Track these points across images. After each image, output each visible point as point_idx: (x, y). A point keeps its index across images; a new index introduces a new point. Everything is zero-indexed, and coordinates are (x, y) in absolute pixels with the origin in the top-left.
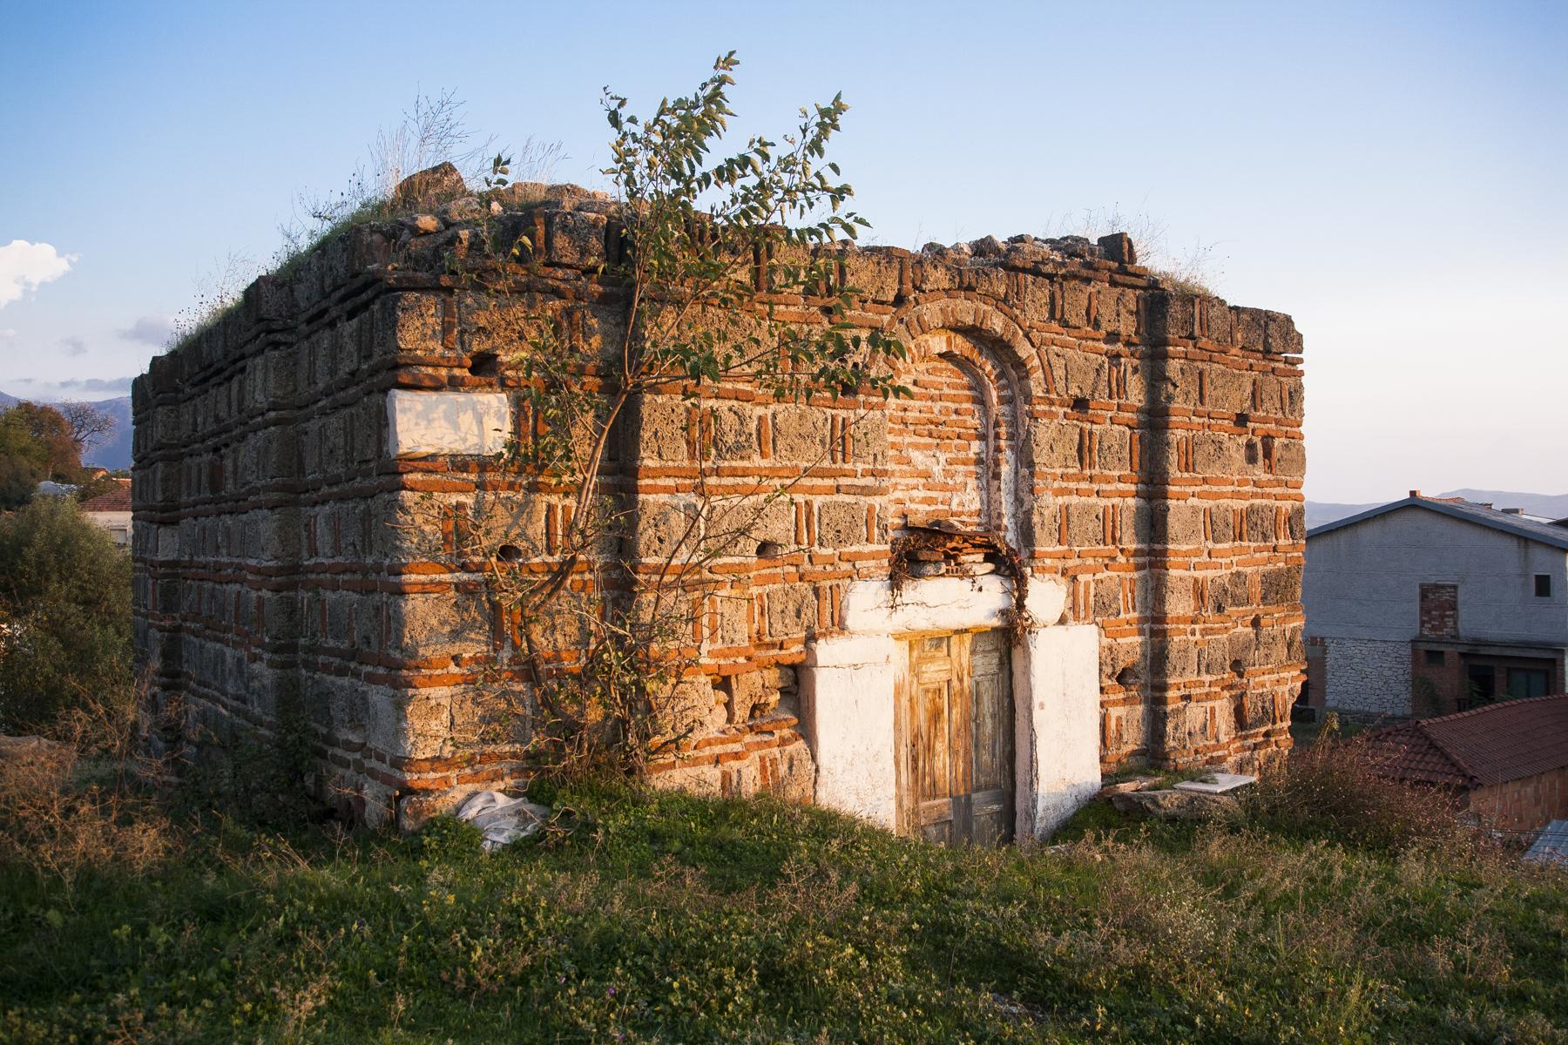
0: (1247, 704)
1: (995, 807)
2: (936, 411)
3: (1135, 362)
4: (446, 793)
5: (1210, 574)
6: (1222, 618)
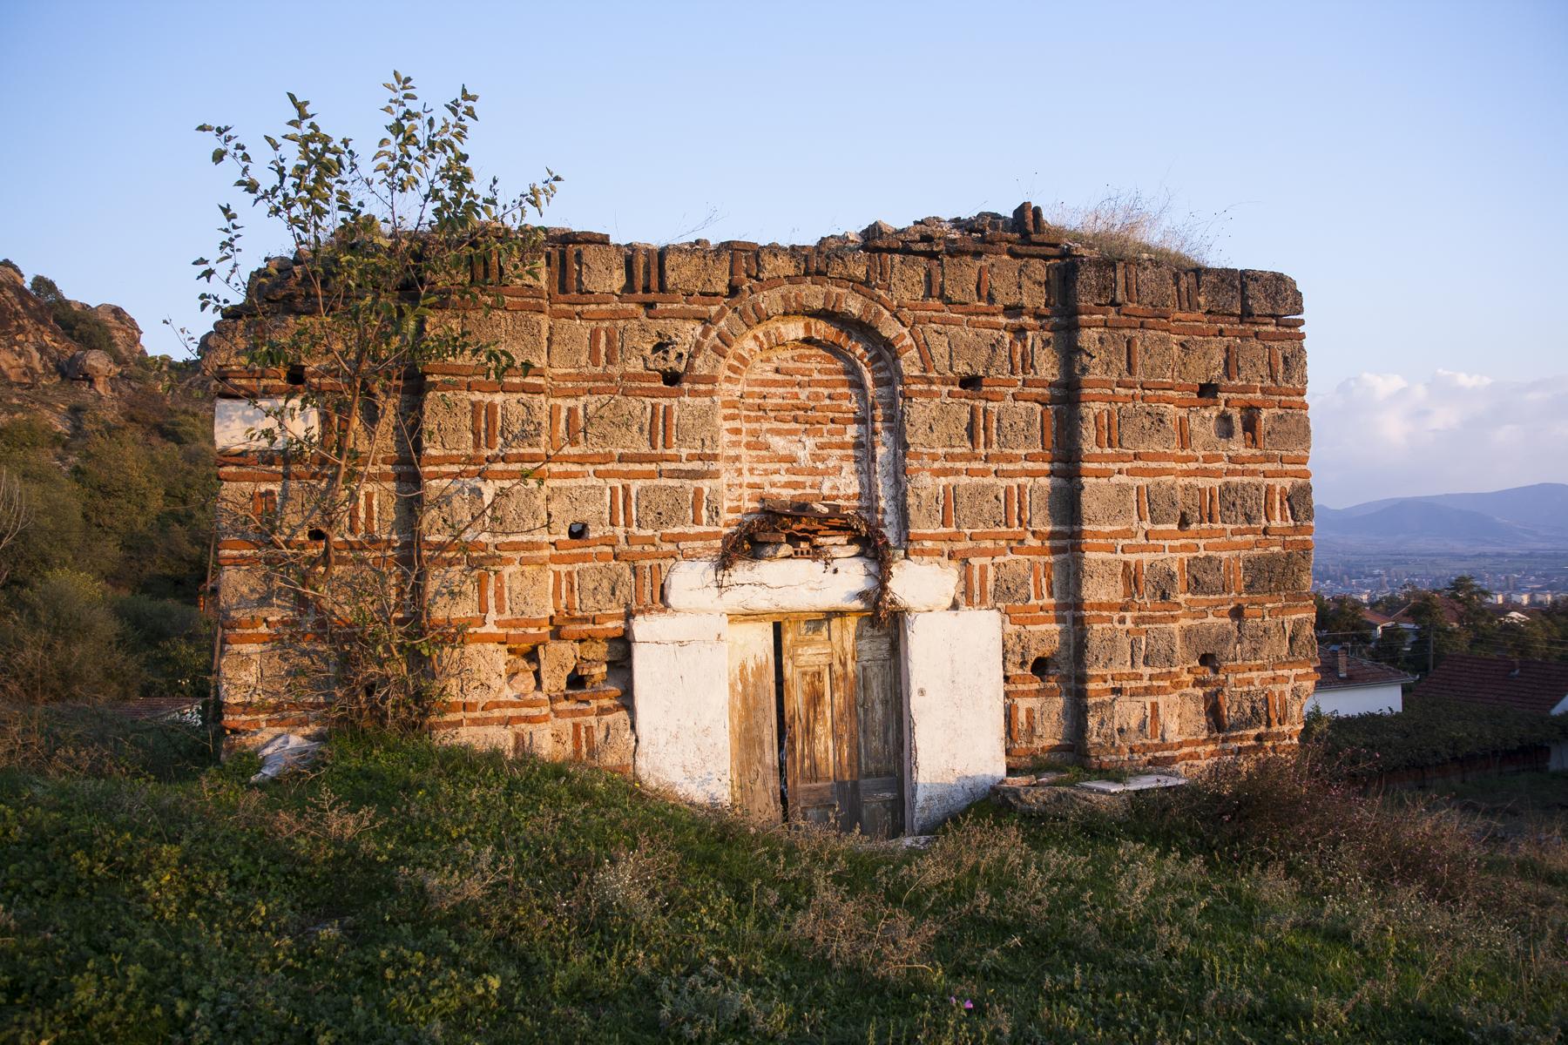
0: (1225, 702)
1: (888, 795)
2: (803, 396)
4: (256, 733)
5: (1147, 557)
6: (1166, 605)
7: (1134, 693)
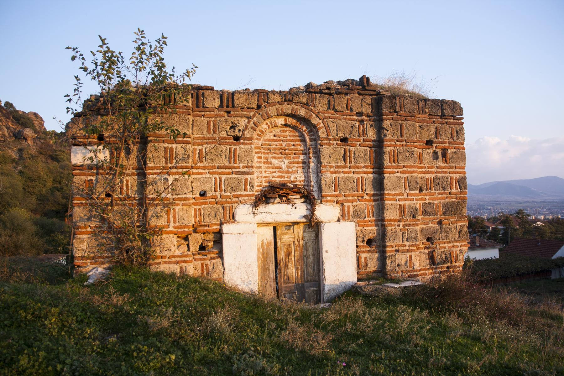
0: (436, 255)
1: (315, 289)
3: (371, 123)
4: (86, 267)
5: (407, 203)
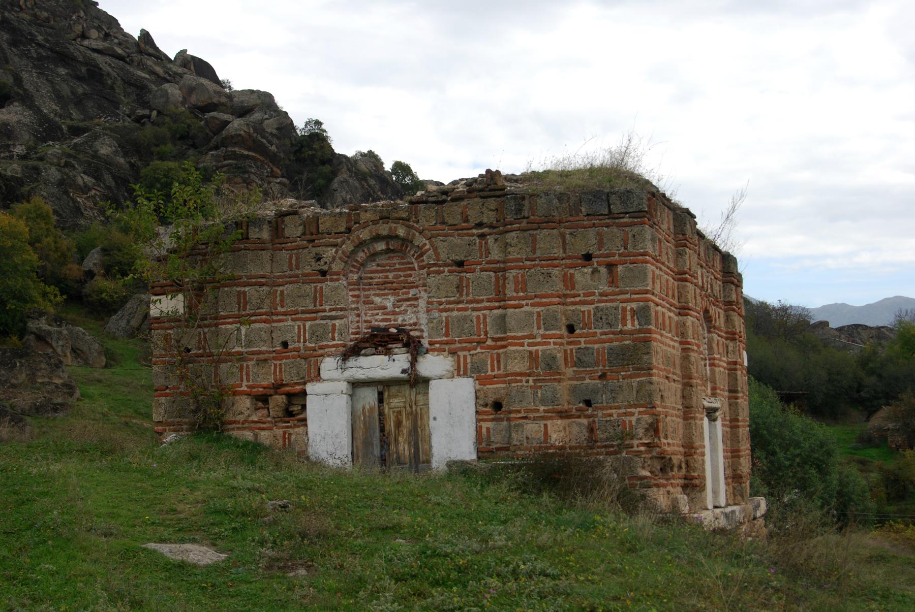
5: (540, 348)
7: (534, 419)
